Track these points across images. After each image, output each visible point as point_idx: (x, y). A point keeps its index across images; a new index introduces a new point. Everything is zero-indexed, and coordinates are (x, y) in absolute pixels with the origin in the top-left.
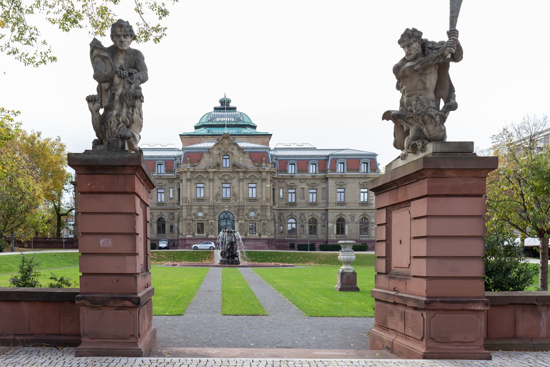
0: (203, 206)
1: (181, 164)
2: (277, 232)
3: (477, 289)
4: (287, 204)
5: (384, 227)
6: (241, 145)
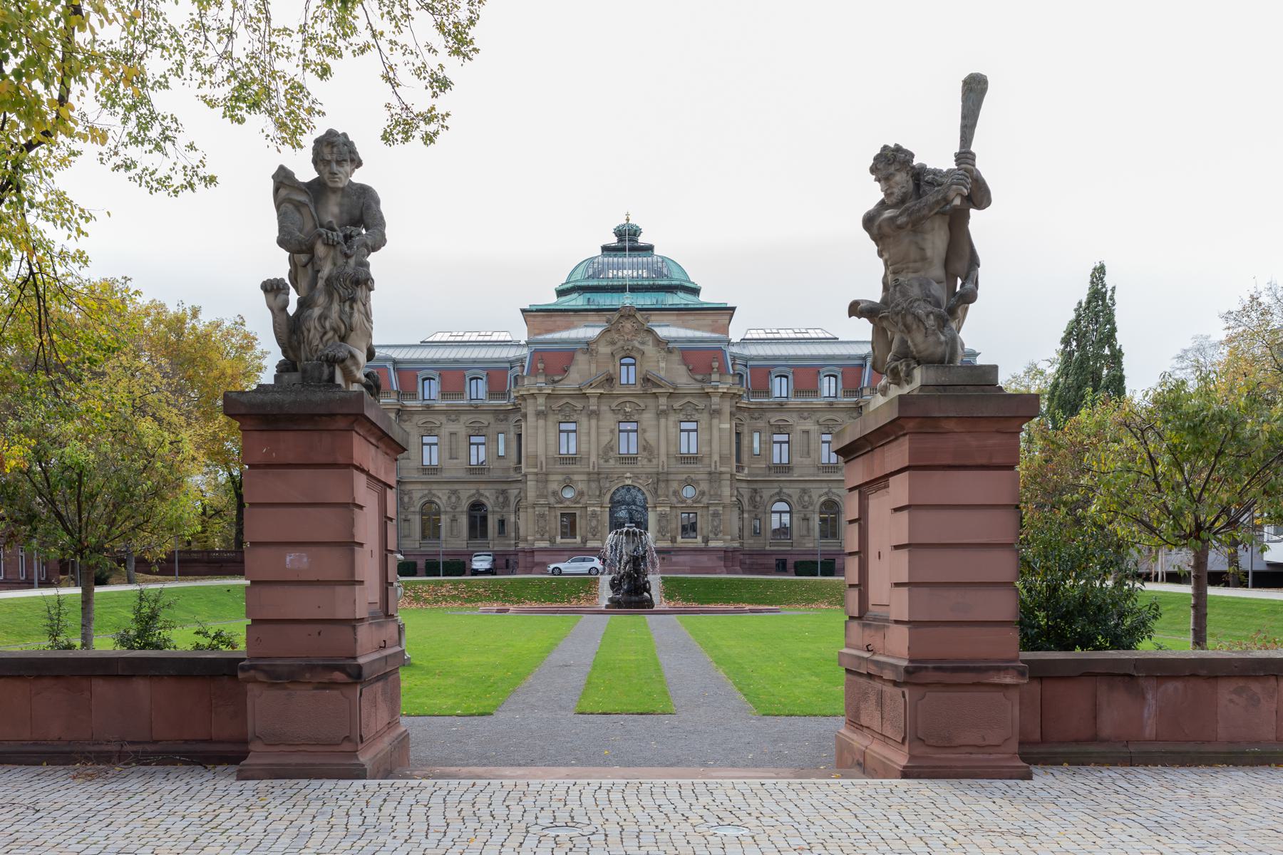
0: (573, 474)
1: (523, 377)
2: (746, 534)
3: (1007, 644)
4: (770, 468)
5: (856, 526)
6: (662, 332)
